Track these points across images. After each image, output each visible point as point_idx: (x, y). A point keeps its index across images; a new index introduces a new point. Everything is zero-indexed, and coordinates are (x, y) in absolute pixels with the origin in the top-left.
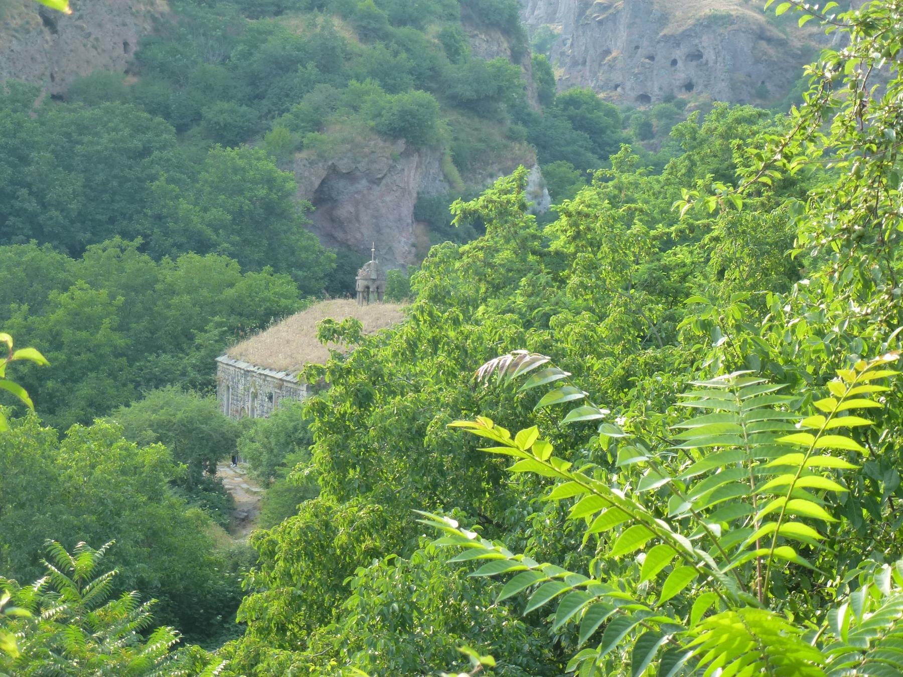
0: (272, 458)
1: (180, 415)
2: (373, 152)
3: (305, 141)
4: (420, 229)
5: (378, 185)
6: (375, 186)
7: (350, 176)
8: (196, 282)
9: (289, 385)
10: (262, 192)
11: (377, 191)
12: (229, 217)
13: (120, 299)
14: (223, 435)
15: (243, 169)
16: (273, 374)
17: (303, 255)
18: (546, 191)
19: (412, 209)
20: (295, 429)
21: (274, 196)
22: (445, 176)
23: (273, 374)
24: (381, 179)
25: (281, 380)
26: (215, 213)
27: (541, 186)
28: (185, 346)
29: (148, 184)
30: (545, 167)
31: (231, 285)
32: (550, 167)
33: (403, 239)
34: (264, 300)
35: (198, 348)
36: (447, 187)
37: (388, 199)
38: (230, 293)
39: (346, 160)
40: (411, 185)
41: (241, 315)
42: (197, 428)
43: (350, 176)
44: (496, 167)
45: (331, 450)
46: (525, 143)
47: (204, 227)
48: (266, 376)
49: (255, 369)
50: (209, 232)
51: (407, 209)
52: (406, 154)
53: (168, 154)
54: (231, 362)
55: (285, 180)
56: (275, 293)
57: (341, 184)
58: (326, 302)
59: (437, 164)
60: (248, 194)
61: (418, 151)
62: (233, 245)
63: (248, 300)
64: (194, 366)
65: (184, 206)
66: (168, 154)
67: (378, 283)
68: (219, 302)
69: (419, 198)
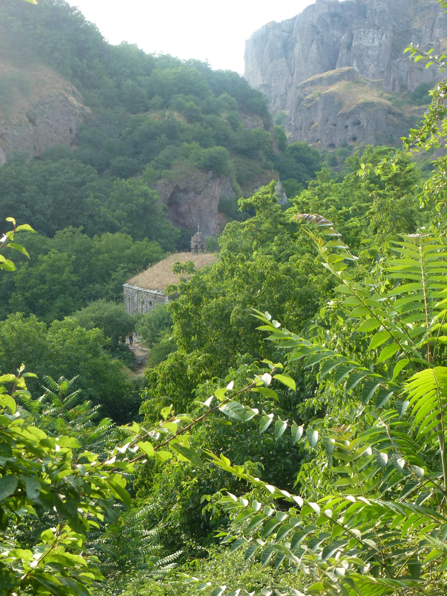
0: (153, 333)
1: (106, 314)
2: (196, 178)
3: (162, 174)
4: (221, 216)
5: (200, 195)
6: (198, 195)
7: (186, 191)
8: (111, 247)
9: (160, 297)
10: (142, 201)
11: (199, 197)
12: (126, 214)
13: (74, 257)
14: (128, 323)
15: (132, 190)
16: (151, 291)
17: (164, 232)
18: (285, 194)
19: (217, 206)
20: (164, 318)
21: (147, 203)
22: (233, 189)
23: (151, 291)
24: (201, 192)
25: (155, 294)
26: (119, 212)
27: (282, 192)
28: (107, 279)
29: (85, 199)
30: (284, 182)
31: (128, 248)
32: (286, 182)
33: (213, 222)
34: (145, 255)
35: (114, 280)
36: (235, 195)
37: (205, 201)
38: (128, 252)
39: (183, 183)
40: (216, 193)
41: (134, 263)
42: (115, 320)
43: (186, 191)
44: (259, 183)
45: (182, 327)
46: (273, 170)
47: (114, 220)
48: (148, 292)
49: (142, 289)
50: (116, 222)
51: (215, 206)
52: (213, 178)
53: (94, 184)
54: (130, 286)
55: (154, 194)
56: (150, 251)
57: (181, 195)
58: (176, 254)
59: (229, 183)
60: (135, 202)
61: (219, 177)
62: (129, 228)
63: (137, 255)
64: (112, 289)
65: (103, 209)
66: (94, 184)
67: (202, 243)
68: (123, 256)
69: (220, 201)
